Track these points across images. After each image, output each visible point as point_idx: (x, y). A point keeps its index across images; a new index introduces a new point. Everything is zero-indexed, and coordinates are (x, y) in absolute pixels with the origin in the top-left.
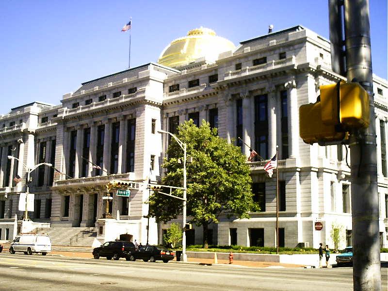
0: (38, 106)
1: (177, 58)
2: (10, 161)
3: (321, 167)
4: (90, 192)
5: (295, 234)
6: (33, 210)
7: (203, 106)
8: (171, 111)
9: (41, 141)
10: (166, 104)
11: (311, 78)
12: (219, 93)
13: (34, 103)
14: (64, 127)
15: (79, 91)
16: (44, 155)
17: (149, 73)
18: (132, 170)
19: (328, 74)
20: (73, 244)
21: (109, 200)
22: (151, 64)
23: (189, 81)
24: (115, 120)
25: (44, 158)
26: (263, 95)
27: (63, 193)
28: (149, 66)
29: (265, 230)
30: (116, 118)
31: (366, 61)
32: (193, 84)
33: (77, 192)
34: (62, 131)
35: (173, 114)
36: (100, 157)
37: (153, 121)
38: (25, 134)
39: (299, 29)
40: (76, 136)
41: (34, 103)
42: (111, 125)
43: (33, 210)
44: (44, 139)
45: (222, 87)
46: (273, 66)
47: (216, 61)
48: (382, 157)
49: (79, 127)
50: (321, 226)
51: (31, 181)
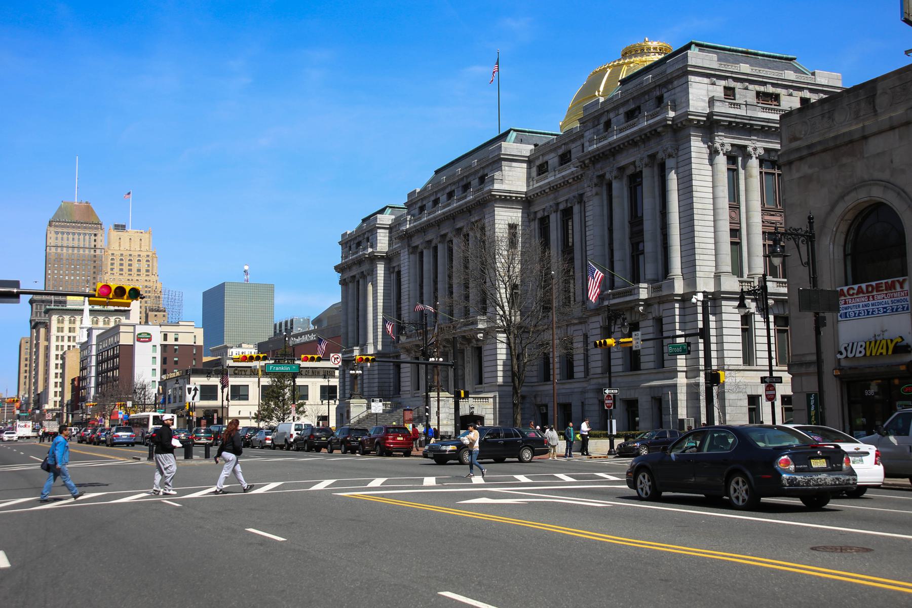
2: (780, 206)
6: (702, 327)
7: (574, 197)
8: (538, 208)
9: (539, 215)
10: (530, 197)
11: (697, 147)
14: (409, 246)
16: (570, 240)
23: (559, 154)
25: (570, 244)
29: (21, 282)
30: (634, 163)
32: (565, 159)
34: (407, 253)
35: (542, 213)
36: (638, 244)
38: (373, 259)
40: (641, 184)
42: (431, 251)
43: (702, 327)
44: (544, 210)
49: (615, 173)
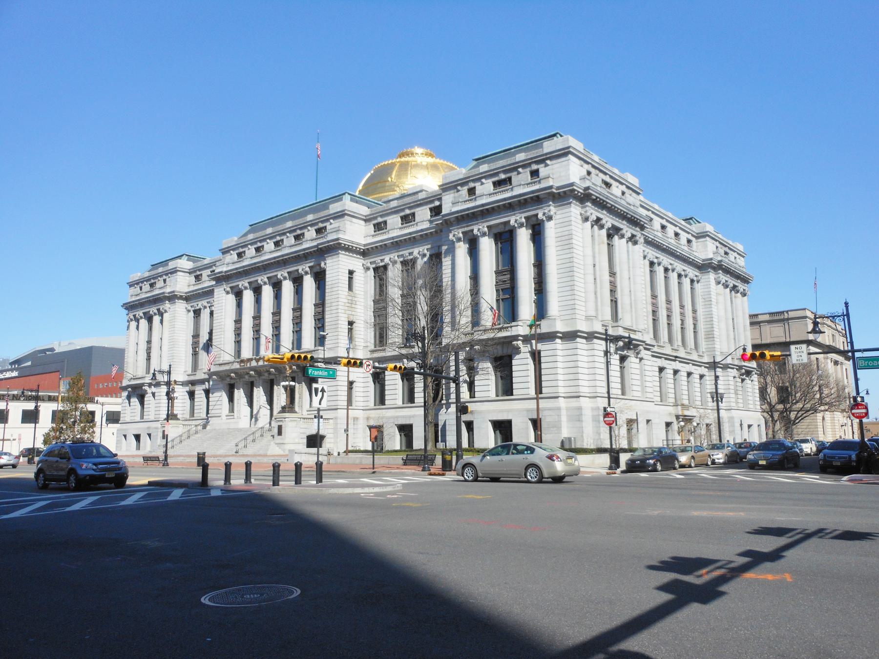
0: (188, 260)
1: (384, 189)
3: (591, 330)
4: (263, 377)
5: (557, 426)
12: (443, 230)
13: (182, 255)
15: (245, 235)
17: (345, 204)
18: (318, 445)
19: (598, 199)
20: (241, 453)
21: (290, 386)
22: (347, 194)
24: (296, 273)
26: (506, 232)
27: (226, 380)
28: (344, 196)
31: (393, 300)
33: (245, 378)
37: (351, 273)
39: (557, 138)
41: (182, 255)
45: (449, 223)
46: (522, 185)
47: (440, 186)
48: (653, 316)
50: (606, 419)
51: (64, 387)
